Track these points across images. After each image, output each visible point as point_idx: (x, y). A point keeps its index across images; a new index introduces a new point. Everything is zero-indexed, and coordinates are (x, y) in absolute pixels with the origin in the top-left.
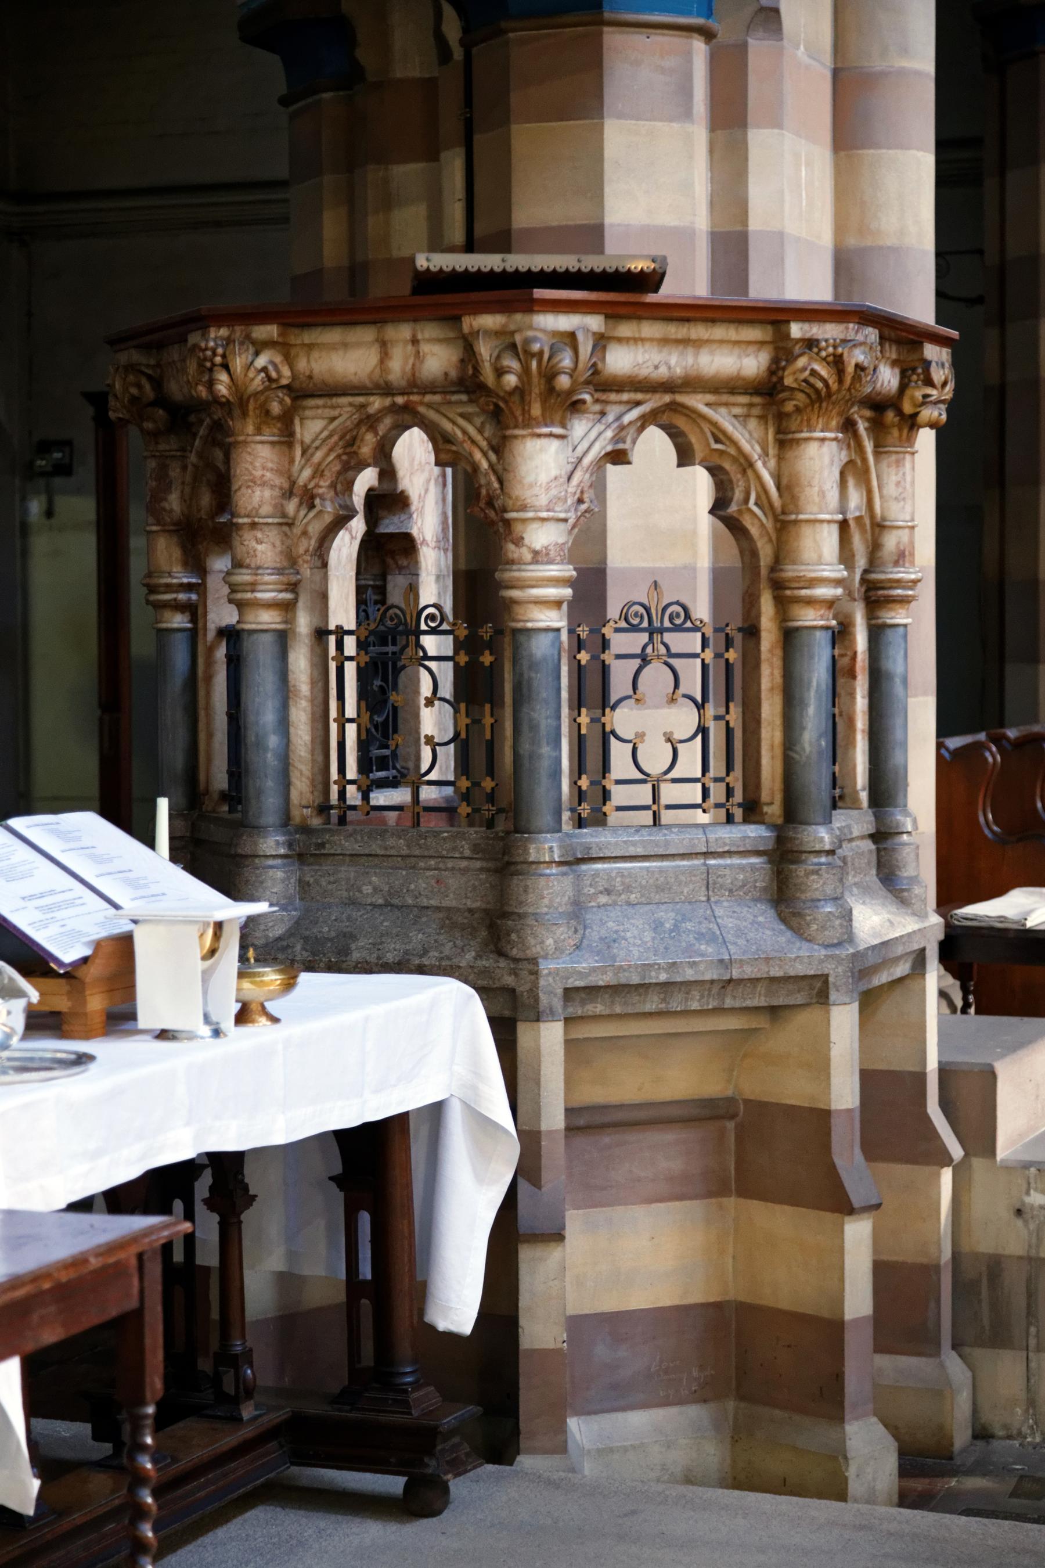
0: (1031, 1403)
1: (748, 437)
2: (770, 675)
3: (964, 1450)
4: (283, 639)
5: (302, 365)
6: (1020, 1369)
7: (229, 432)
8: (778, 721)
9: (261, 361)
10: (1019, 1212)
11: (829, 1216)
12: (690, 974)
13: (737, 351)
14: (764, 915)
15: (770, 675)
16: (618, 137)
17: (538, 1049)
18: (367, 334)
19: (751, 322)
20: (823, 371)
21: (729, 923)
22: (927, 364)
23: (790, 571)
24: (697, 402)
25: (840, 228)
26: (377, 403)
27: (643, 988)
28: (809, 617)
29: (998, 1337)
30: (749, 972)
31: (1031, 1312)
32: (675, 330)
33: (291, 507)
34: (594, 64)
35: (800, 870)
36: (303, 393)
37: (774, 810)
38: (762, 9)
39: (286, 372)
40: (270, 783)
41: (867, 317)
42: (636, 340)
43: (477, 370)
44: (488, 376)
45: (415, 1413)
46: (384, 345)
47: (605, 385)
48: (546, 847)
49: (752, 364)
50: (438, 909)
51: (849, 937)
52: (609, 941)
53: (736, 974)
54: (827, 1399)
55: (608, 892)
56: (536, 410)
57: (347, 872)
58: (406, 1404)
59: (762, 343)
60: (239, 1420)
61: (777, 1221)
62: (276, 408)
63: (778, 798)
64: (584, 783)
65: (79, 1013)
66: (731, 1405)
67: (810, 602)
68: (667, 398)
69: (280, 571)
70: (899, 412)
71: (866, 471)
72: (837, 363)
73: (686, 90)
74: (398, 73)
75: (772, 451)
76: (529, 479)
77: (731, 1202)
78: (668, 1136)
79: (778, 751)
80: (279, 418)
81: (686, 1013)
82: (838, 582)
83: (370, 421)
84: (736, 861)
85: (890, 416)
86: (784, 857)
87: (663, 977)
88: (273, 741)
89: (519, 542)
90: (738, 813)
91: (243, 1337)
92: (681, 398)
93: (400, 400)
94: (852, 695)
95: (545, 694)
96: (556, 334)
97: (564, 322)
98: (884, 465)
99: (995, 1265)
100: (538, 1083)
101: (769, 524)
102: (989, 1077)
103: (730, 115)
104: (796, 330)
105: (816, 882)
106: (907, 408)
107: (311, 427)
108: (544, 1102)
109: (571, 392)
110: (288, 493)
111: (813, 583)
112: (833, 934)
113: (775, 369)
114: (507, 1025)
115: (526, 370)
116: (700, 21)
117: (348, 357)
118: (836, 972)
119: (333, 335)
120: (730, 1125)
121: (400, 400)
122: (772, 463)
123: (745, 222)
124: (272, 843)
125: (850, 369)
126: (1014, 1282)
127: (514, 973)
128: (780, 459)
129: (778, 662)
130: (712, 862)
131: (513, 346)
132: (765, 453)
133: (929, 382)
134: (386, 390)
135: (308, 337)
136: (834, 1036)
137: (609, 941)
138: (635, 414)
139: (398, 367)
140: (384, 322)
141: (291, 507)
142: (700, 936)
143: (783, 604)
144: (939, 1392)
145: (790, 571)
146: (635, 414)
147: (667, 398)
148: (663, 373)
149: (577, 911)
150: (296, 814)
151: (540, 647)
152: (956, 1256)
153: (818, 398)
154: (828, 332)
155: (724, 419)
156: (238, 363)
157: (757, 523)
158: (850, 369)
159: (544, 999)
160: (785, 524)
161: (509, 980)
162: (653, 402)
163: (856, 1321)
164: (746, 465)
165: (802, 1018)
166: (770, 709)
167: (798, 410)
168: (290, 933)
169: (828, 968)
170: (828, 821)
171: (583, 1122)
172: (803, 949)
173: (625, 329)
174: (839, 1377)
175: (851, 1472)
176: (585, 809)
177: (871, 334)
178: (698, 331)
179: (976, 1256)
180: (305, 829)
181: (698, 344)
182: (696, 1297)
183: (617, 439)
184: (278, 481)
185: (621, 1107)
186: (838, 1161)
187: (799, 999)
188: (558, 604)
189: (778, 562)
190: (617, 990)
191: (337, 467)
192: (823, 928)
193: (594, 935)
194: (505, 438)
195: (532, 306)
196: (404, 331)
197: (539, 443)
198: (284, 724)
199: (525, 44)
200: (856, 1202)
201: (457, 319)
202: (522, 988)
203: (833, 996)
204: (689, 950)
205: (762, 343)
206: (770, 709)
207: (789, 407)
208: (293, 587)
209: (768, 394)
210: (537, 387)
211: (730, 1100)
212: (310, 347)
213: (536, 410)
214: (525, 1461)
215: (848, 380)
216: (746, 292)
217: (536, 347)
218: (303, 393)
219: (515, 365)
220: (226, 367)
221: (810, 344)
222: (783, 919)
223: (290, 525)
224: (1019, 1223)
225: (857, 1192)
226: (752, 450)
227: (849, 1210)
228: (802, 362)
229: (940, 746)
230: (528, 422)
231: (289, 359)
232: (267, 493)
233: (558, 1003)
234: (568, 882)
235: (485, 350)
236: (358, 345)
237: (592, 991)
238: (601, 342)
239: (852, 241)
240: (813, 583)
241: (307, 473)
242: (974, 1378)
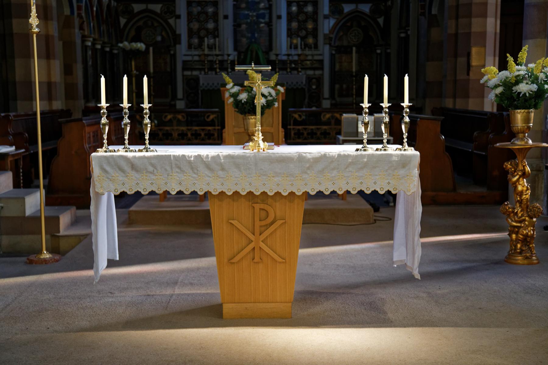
239: (483, 49)
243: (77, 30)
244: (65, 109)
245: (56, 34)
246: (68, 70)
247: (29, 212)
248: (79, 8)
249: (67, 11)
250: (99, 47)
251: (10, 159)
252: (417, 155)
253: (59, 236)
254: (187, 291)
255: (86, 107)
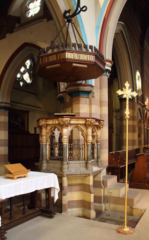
0: (110, 208)
1: (84, 128)
2: (86, 148)
3: (104, 211)
4: (46, 145)
5: (47, 123)
6: (109, 205)
7: (42, 128)
8: (86, 152)
9: (43, 122)
10: (109, 192)
11: (90, 194)
12: (78, 173)
13: (82, 121)
14: (85, 168)
15: (86, 148)
16: (81, 105)
17: (64, 180)
18: (51, 120)
19: (83, 119)
20: (89, 123)
21: (82, 169)
22: (101, 123)
23: (87, 140)
24: (79, 126)
25: (100, 113)
26: (53, 126)
27: (73, 175)
28: (89, 144)
29: (107, 202)
30: (83, 173)
31: (110, 200)
32: (76, 120)
33: (47, 134)
34: (79, 100)
35: (88, 165)
36: (47, 125)
37: (86, 160)
38: (93, 96)
39: (46, 123)
40: (45, 157)
41: (94, 118)
42: (73, 120)
43: (59, 123)
44: (60, 124)
45: (50, 210)
46: (53, 121)
47: (71, 124)
48: (65, 163)
49: (84, 122)
50: (57, 167)
51: (92, 170)
52: (71, 171)
53: (82, 173)
54: (90, 208)
55: (71, 166)
56: (64, 126)
57: (51, 164)
58: (50, 209)
59: (84, 121)
60: (36, 210)
61: (86, 194)
62: (45, 126)
63: (86, 159)
64: (70, 157)
65: (14, 178)
66: (82, 208)
67: (89, 142)
68: (76, 125)
69: (45, 139)
70: (99, 127)
71: (96, 131)
72: (91, 122)
73: (87, 102)
74: (67, 102)
75: (86, 130)
76: (64, 132)
77: (83, 192)
78: (77, 186)
79: (87, 155)
80: (46, 127)
81: (78, 177)
82: (91, 141)
83: (53, 127)
84: (83, 164)
85: (98, 127)
86: (87, 163)
87: (75, 174)
88: (45, 153)
89: (63, 137)
90: (83, 160)
91: (37, 203)
92: (78, 125)
93: (55, 125)
94: (95, 150)
95: (65, 150)
96: (66, 120)
97: (67, 119)
98: (98, 131)
99: (107, 196)
100: (64, 182)
101: (86, 136)
102: (107, 181)
103: (90, 104)
104: (87, 120)
105: (89, 166)
106: (99, 126)
107: (49, 128)
108: (64, 184)
109: (67, 125)
110: (46, 133)
111: (89, 141)
112: (90, 170)
113: (86, 123)
114: (60, 178)
115: (63, 123)
116: (87, 97)
117: (50, 122)
118: (91, 173)
119: (49, 120)
120: (83, 185)
121: (55, 125)
122: (86, 131)
123: (91, 112)
124: (45, 161)
125: (92, 123)
126: (109, 198)
127: (62, 173)
128: (87, 130)
129: (86, 147)
130: (80, 164)
131: (62, 121)
132: (85, 130)
133: (101, 124)
134: (53, 125)
135: (47, 120)
136: (90, 179)
137: (71, 171)
138: (74, 126)
139: (54, 123)
140: (53, 119)
141: (47, 134)
142: (79, 170)
143: (87, 142)
144: (101, 207)
145: (87, 140)
146: (74, 126)
147: (76, 125)
148: (76, 123)
149: (68, 168)
150: (47, 159)
151: (65, 146)
152: (104, 195)
153: (89, 125)
154: (90, 120)
155: (82, 127)
156: (42, 123)
157: (85, 136)
158: (92, 123)
159: (64, 175)
160: (87, 136)
161: (62, 174)
162: (75, 126)
163: (92, 202)
164: (84, 131)
165: (88, 177)
166: (86, 151)
167: (88, 126)
168: (46, 169)
169: (90, 173)
170: (90, 161)
171: (69, 185)
172: (88, 171)
173: (72, 120)
174: (90, 207)
175: (91, 215)
176: (70, 159)
177: (94, 120)
178: (79, 120)
179: (105, 196)
180: (48, 160)
181: (79, 121)
182: (80, 199)
183: (72, 129)
184: (46, 132)
185: (73, 184)
186: (90, 189)
187: (88, 175)
188: (67, 142)
189: (87, 139)
190: (71, 175)
191: (50, 131)
192: (90, 170)
193: (69, 170)
194: (62, 129)
195: (63, 118)
196: (55, 120)
197: (65, 129)
198: (46, 152)
199: (74, 99)
200: (92, 192)
201: (58, 119)
202: (63, 174)
203: (90, 175)
204: (78, 171)
205: (84, 121)
206: (86, 151)
207: (87, 126)
208: (47, 141)
209: (85, 125)
210: (64, 125)
211: (83, 183)
212: (48, 121)
213: (64, 126)
214: (63, 213)
215: (92, 124)
216: (79, 116)
217: (64, 121)
218: (47, 125)
219: (62, 122)
220: (41, 123)
221: (88, 121)
222: (86, 169)
223: (47, 136)
224: (109, 193)
225: (92, 192)
226: (84, 130)
227: (91, 193)
228: (88, 122)
229: (109, 154)
230: (64, 127)
231: (46, 122)
232: (45, 133)
233: (66, 176)
234: (67, 165)
235: (60, 121)
236: (51, 121)
237: (69, 175)
238: (70, 121)
239: (101, 114)
240: (89, 141)
241: (48, 131)
242: (105, 206)
243: (142, 124)
244: (138, 148)
245: (136, 125)
246: (139, 136)
247: (121, 195)
248: (143, 117)
249: (140, 118)
250: (146, 128)
251: (98, 220)
252: (63, 83)
253: (133, 208)
254: (115, 57)
255: (144, 147)
